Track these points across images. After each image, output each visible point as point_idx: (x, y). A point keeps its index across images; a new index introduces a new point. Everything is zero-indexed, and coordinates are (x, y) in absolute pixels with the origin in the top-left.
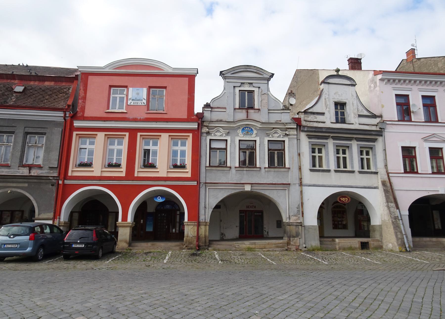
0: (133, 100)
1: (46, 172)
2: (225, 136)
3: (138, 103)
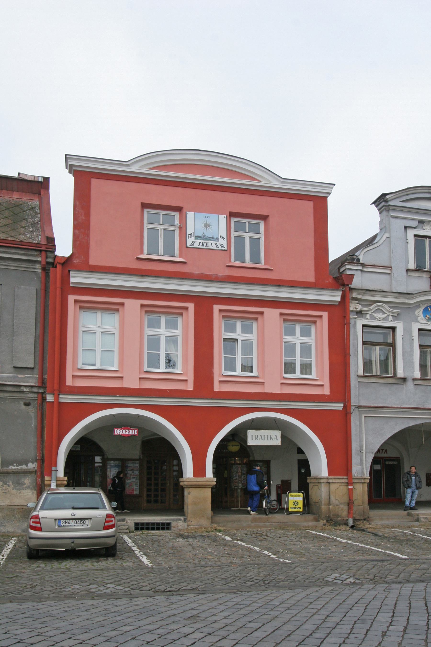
0: (197, 237)
1: (8, 377)
2: (391, 321)
3: (210, 244)
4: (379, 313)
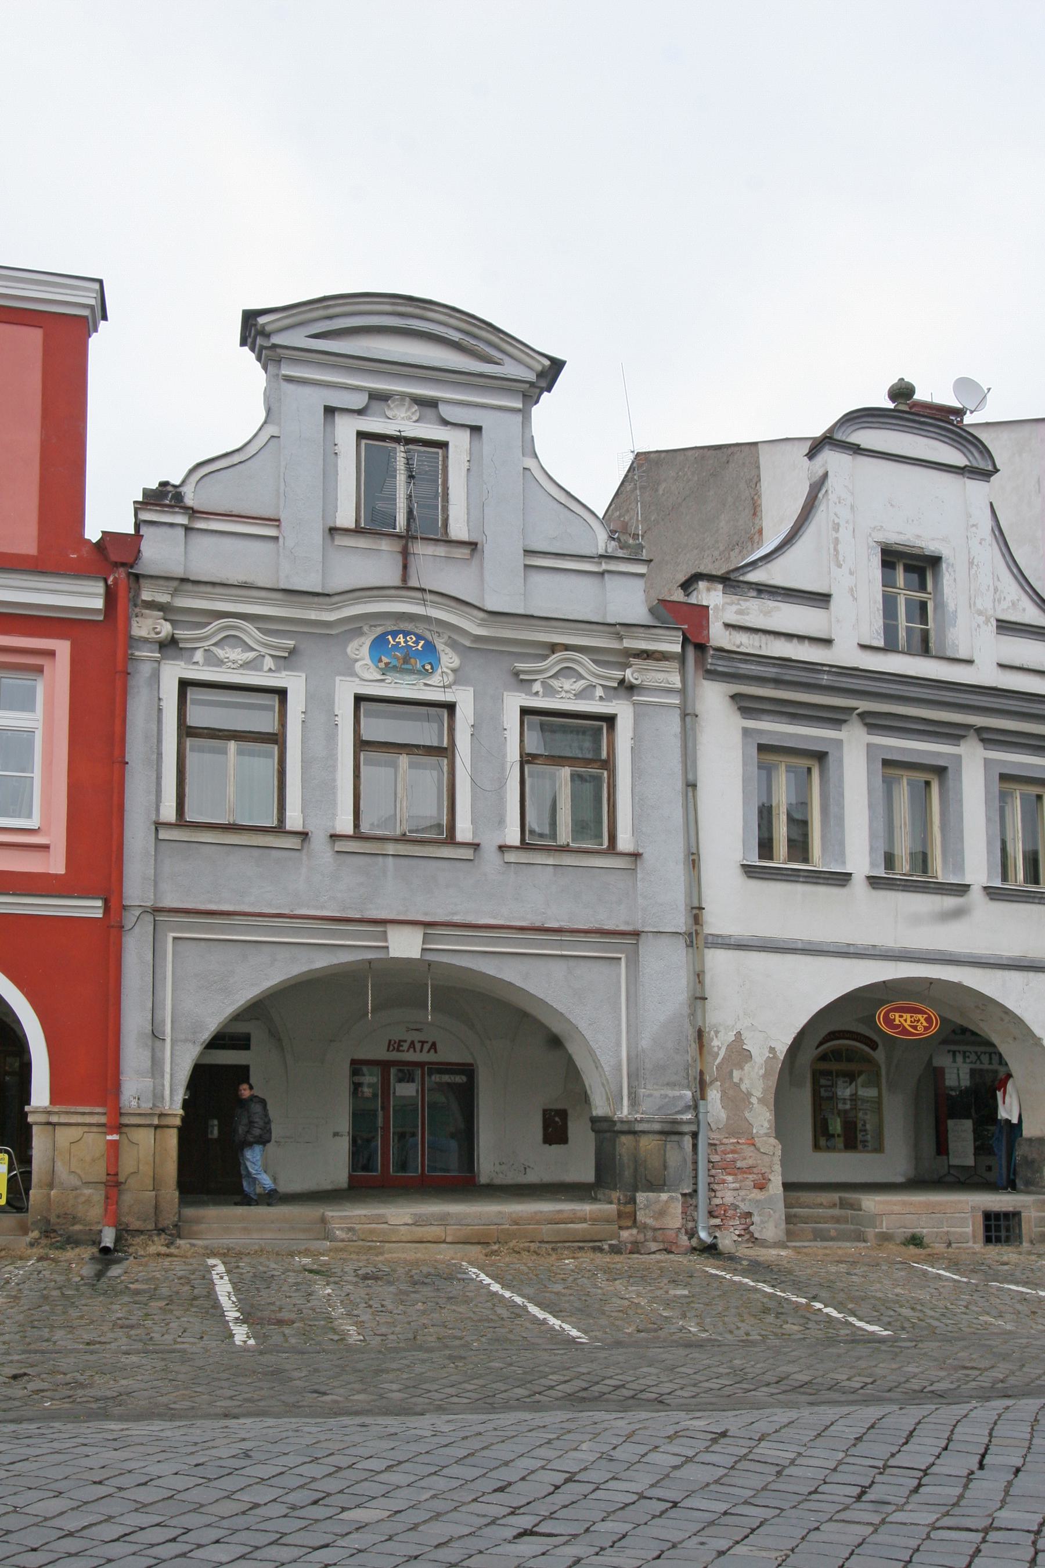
2: (270, 670)
4: (234, 647)
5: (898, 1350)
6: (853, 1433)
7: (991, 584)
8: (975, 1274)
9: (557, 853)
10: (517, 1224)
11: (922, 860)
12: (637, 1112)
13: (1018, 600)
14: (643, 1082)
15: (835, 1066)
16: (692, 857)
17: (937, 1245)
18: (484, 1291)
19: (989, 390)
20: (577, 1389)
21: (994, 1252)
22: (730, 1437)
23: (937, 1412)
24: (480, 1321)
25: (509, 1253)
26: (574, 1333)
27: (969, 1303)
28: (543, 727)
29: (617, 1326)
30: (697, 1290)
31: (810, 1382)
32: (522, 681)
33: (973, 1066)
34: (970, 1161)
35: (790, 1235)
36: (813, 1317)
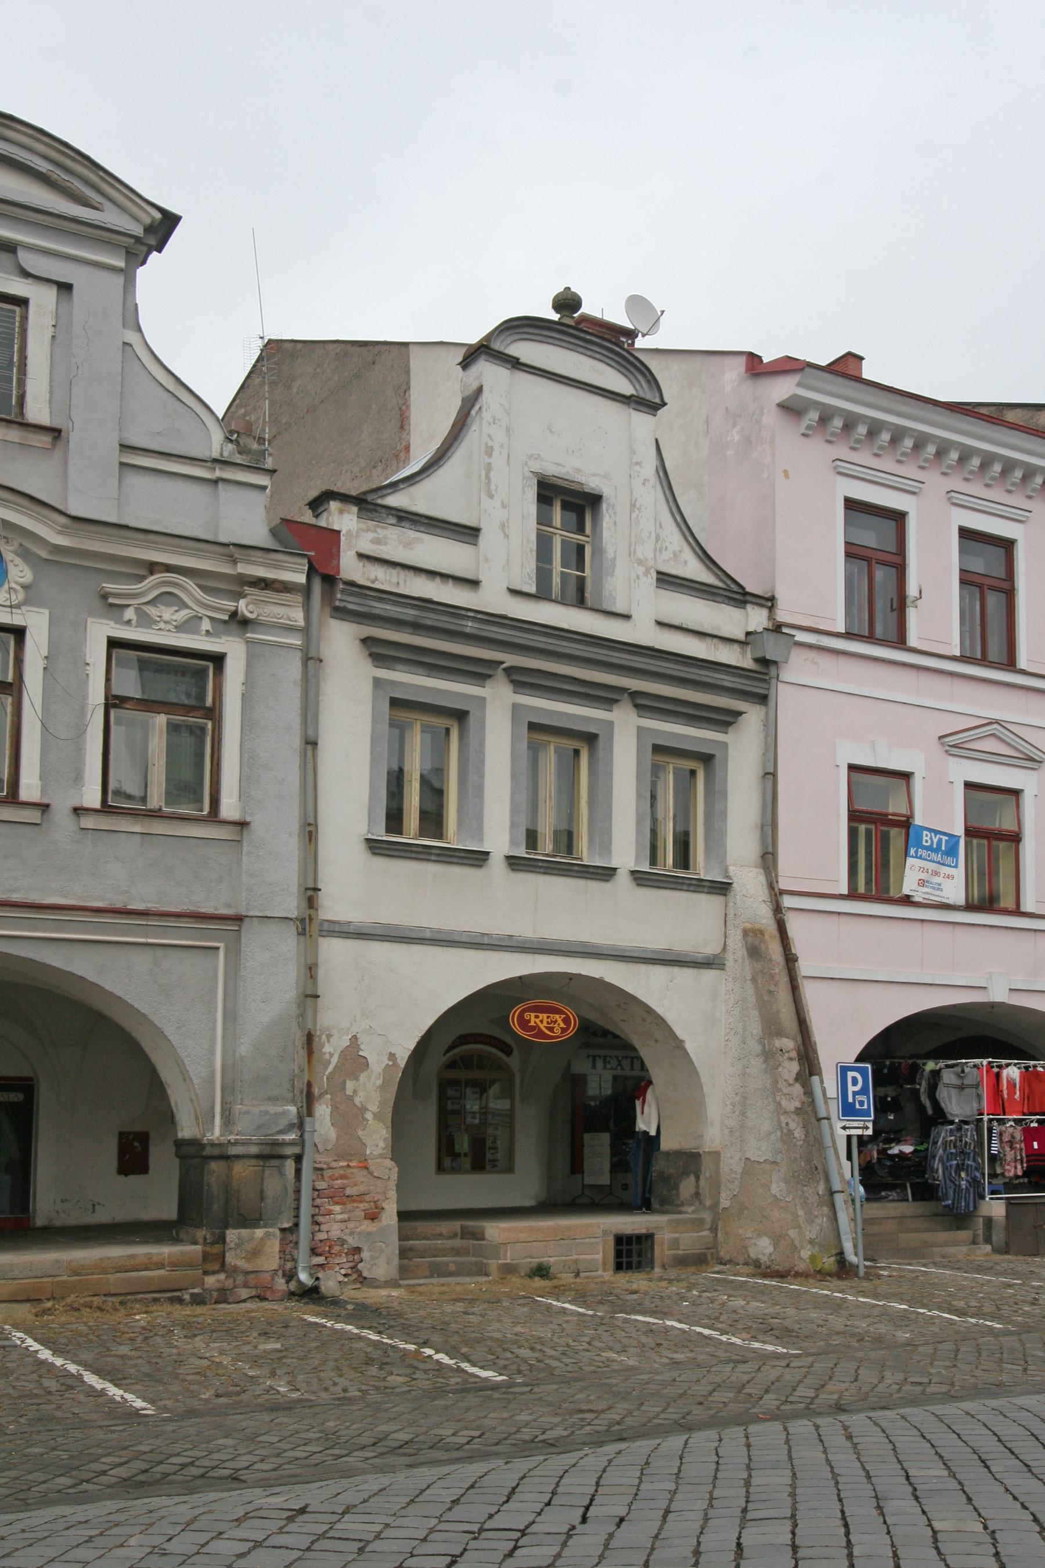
5: (511, 1397)
6: (448, 1497)
7: (653, 532)
8: (601, 1306)
9: (147, 819)
10: (78, 1274)
11: (567, 840)
12: (231, 1133)
13: (680, 552)
14: (240, 1097)
15: (462, 1075)
16: (308, 829)
17: (565, 1275)
18: (30, 1359)
19: (663, 312)
20: (135, 1471)
21: (623, 1280)
22: (310, 1512)
23: (546, 1463)
24: (20, 1397)
25: (66, 1311)
26: (139, 1403)
27: (592, 1339)
28: (143, 666)
29: (192, 1392)
30: (292, 1342)
31: (411, 1441)
32: (111, 605)
33: (615, 1072)
34: (605, 1180)
35: (404, 1271)
36: (421, 1366)
